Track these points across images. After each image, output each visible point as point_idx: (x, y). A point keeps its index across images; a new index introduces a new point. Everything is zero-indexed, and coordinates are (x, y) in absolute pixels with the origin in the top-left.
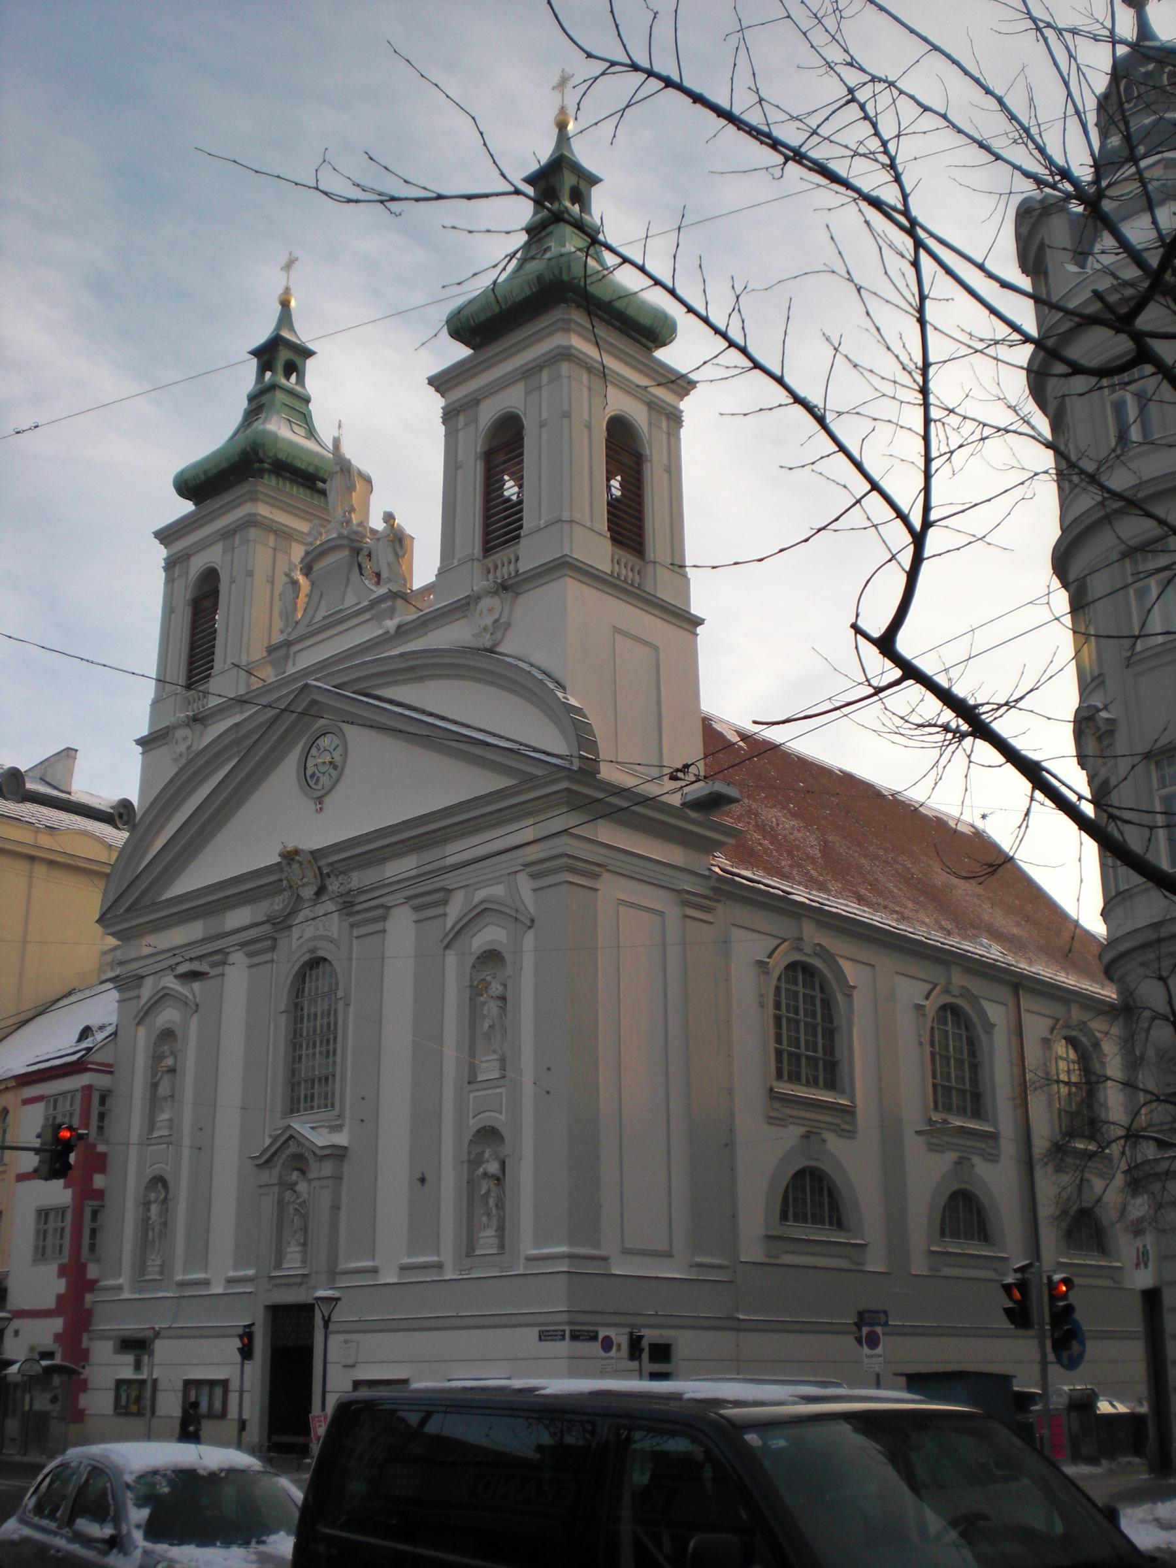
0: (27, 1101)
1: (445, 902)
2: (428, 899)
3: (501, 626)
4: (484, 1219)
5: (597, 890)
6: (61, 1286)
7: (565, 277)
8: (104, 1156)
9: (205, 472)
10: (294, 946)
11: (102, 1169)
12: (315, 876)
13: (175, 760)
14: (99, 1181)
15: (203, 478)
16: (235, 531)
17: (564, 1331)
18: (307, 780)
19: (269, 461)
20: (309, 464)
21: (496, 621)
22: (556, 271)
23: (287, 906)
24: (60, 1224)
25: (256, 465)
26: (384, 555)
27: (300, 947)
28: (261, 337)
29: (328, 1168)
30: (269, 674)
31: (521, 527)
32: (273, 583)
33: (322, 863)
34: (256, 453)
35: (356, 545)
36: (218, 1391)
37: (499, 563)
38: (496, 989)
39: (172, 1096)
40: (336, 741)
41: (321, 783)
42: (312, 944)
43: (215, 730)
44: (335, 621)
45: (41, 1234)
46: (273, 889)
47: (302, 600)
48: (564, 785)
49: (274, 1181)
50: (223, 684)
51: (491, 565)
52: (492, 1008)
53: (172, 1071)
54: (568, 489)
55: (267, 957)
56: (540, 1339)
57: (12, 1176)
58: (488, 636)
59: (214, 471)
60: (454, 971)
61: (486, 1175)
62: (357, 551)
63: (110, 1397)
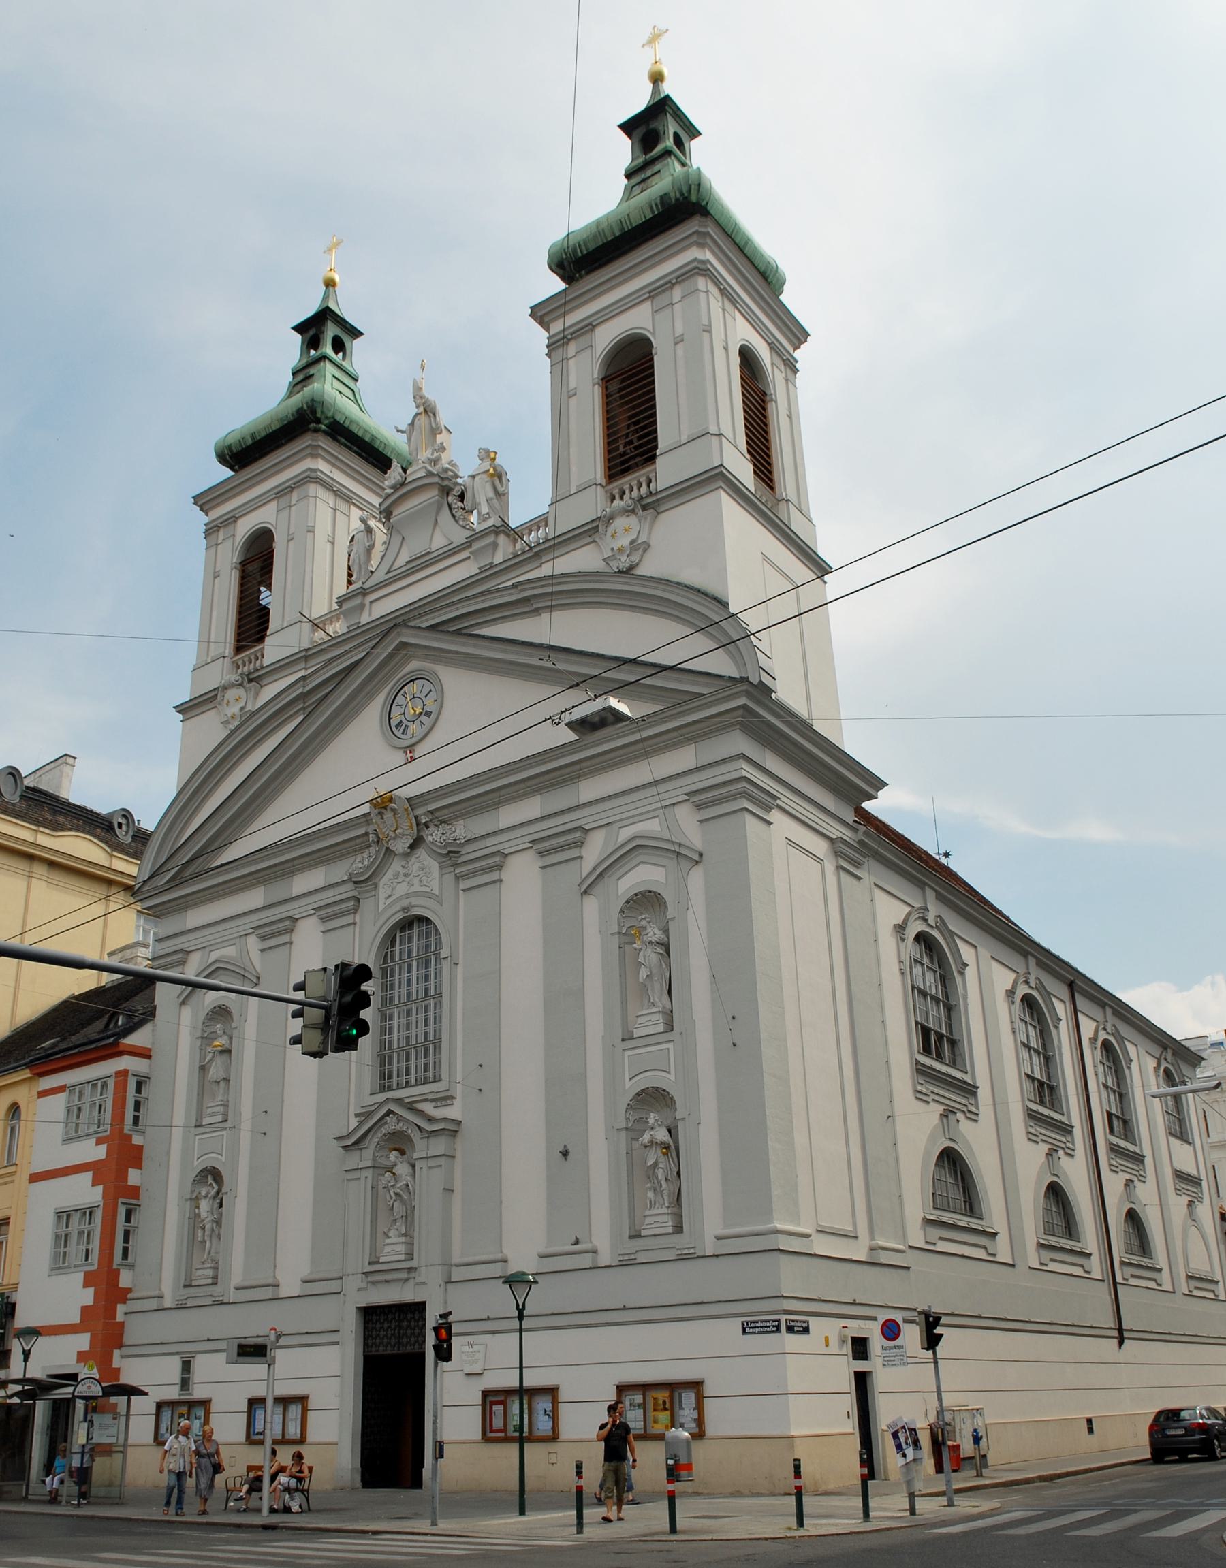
0: (42, 1094)
1: (580, 844)
2: (557, 845)
3: (640, 547)
4: (650, 1194)
5: (770, 823)
6: (88, 1297)
7: (694, 198)
8: (140, 1148)
9: (253, 435)
10: (381, 907)
11: (138, 1164)
12: (411, 827)
13: (226, 723)
14: (134, 1177)
15: (250, 442)
16: (292, 489)
17: (779, 1321)
18: (393, 727)
19: (326, 422)
20: (366, 431)
21: (633, 542)
22: (685, 190)
23: (369, 867)
24: (85, 1227)
25: (313, 425)
26: (482, 493)
27: (390, 906)
28: (309, 310)
29: (439, 1146)
30: (338, 628)
31: (656, 447)
32: (333, 543)
33: (419, 812)
34: (314, 412)
35: (446, 483)
36: (688, 1398)
37: (626, 487)
38: (654, 933)
39: (227, 1080)
40: (428, 686)
41: (410, 732)
42: (405, 903)
43: (271, 690)
44: (422, 563)
45: (62, 1240)
46: (358, 845)
47: (379, 548)
48: (743, 701)
49: (369, 1164)
50: (274, 648)
51: (616, 492)
52: (650, 956)
53: (227, 1051)
54: (698, 411)
55: (349, 919)
56: (744, 1332)
57: (26, 1177)
58: (624, 558)
59: (263, 434)
60: (596, 919)
61: (653, 1143)
62: (446, 491)
63: (474, 1417)
